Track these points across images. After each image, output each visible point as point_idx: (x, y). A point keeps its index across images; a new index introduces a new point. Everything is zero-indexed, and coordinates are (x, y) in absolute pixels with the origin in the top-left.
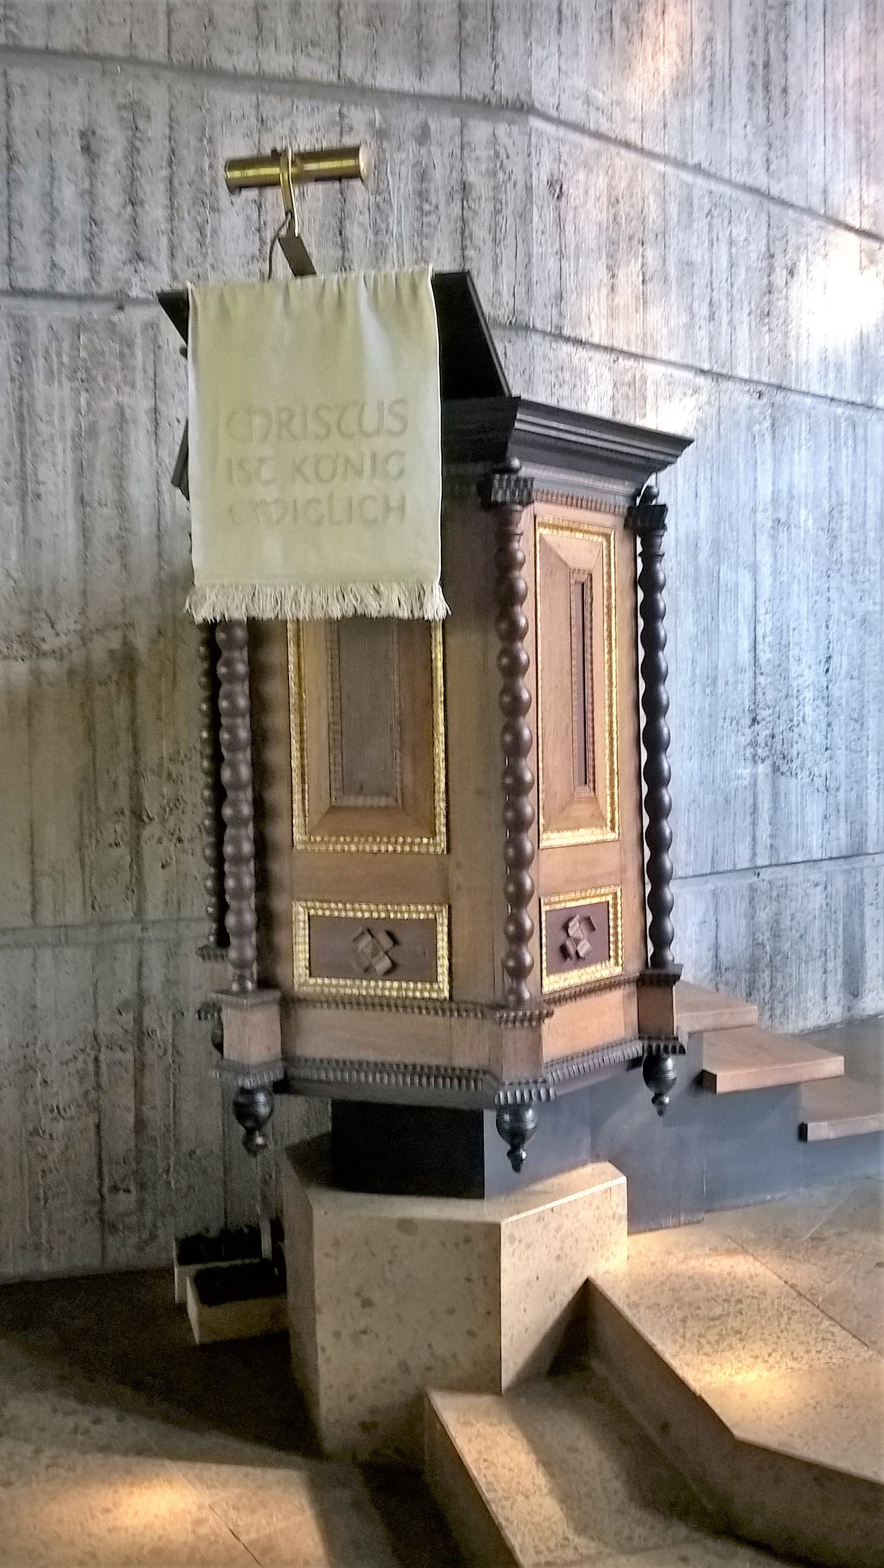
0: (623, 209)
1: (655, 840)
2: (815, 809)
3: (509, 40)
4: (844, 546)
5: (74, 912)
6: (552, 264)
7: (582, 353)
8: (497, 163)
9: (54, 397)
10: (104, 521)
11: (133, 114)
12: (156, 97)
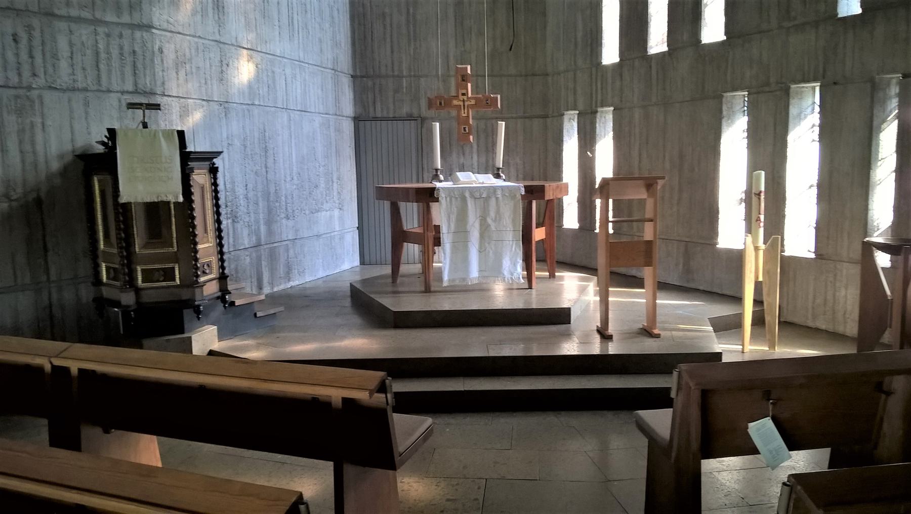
0: (179, 53)
1: (221, 245)
2: (246, 232)
3: (145, 6)
4: (248, 149)
5: (27, 280)
6: (161, 73)
7: (170, 99)
8: (144, 44)
11: (29, 28)
12: (36, 22)
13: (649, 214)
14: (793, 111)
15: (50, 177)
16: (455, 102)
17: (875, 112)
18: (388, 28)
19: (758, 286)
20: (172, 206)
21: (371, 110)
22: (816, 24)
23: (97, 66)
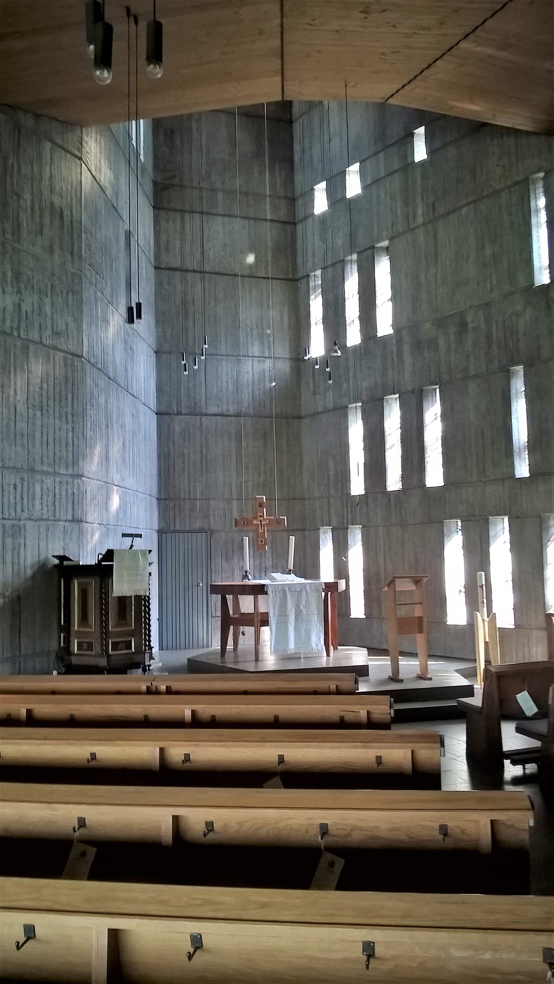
9: (9, 541)
10: (16, 568)
13: (416, 599)
14: (492, 533)
15: (26, 580)
16: (255, 522)
17: (543, 535)
18: (187, 465)
19: (486, 643)
20: (133, 598)
21: (172, 525)
22: (503, 480)
23: (54, 503)
